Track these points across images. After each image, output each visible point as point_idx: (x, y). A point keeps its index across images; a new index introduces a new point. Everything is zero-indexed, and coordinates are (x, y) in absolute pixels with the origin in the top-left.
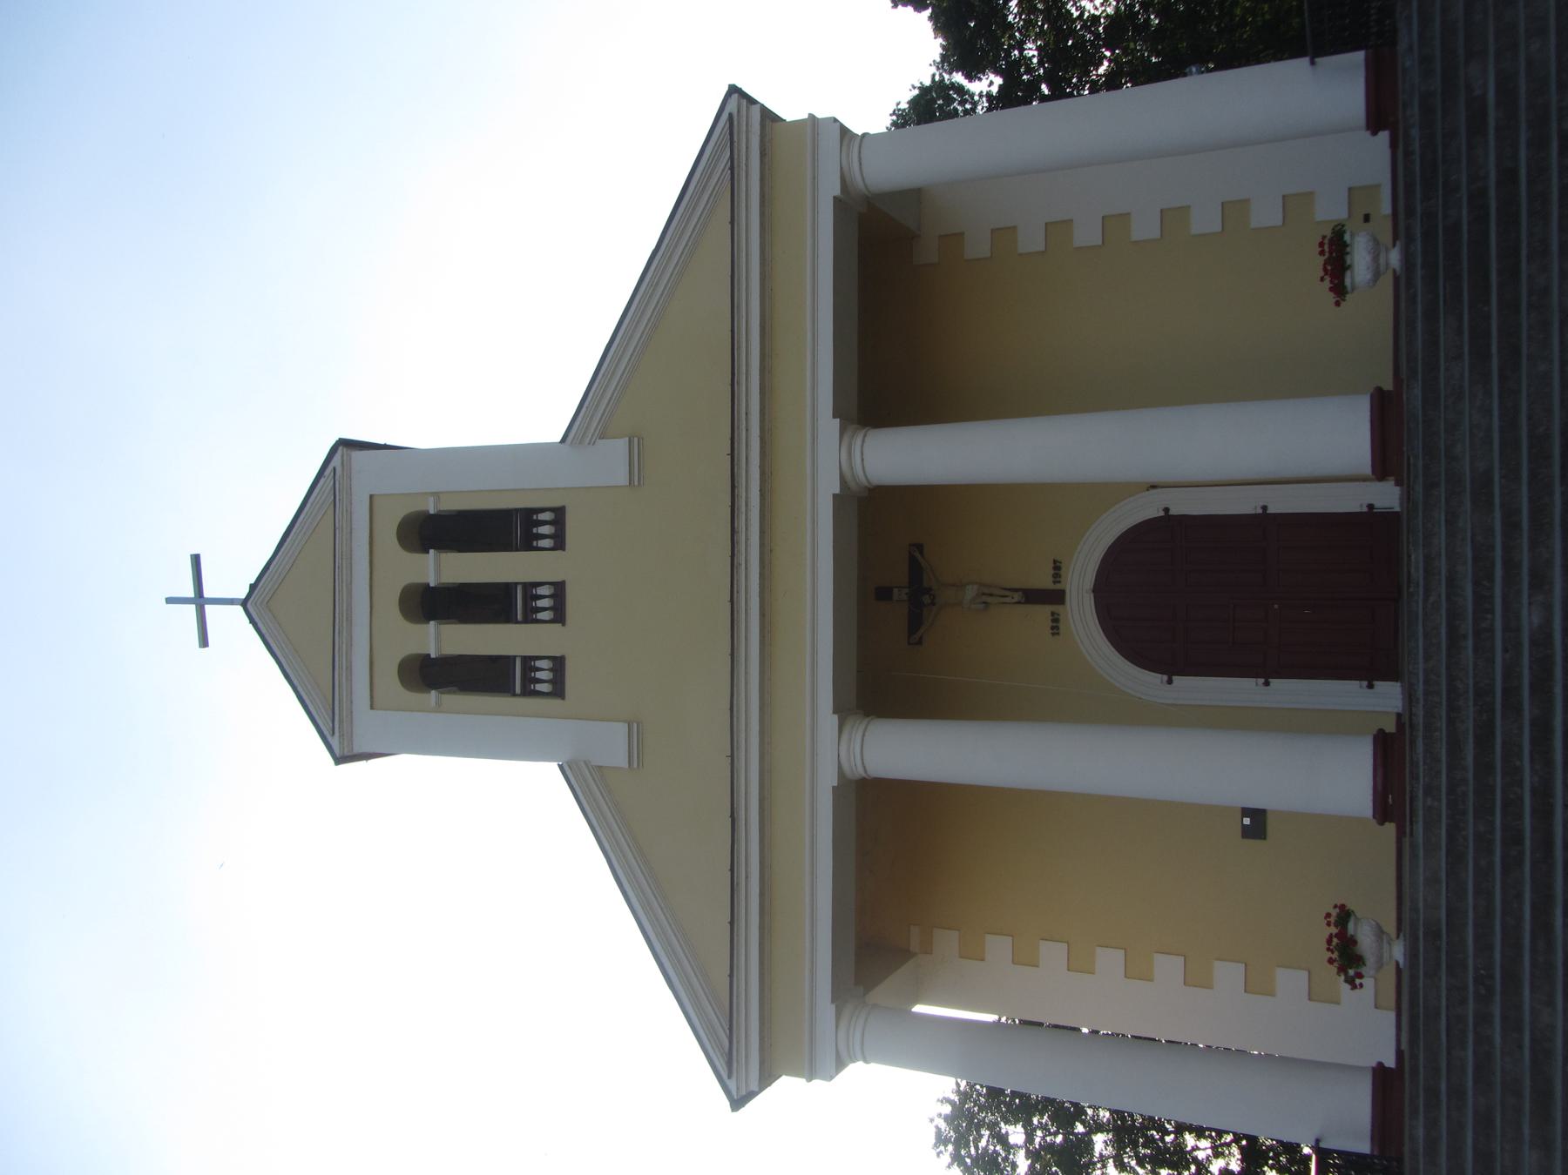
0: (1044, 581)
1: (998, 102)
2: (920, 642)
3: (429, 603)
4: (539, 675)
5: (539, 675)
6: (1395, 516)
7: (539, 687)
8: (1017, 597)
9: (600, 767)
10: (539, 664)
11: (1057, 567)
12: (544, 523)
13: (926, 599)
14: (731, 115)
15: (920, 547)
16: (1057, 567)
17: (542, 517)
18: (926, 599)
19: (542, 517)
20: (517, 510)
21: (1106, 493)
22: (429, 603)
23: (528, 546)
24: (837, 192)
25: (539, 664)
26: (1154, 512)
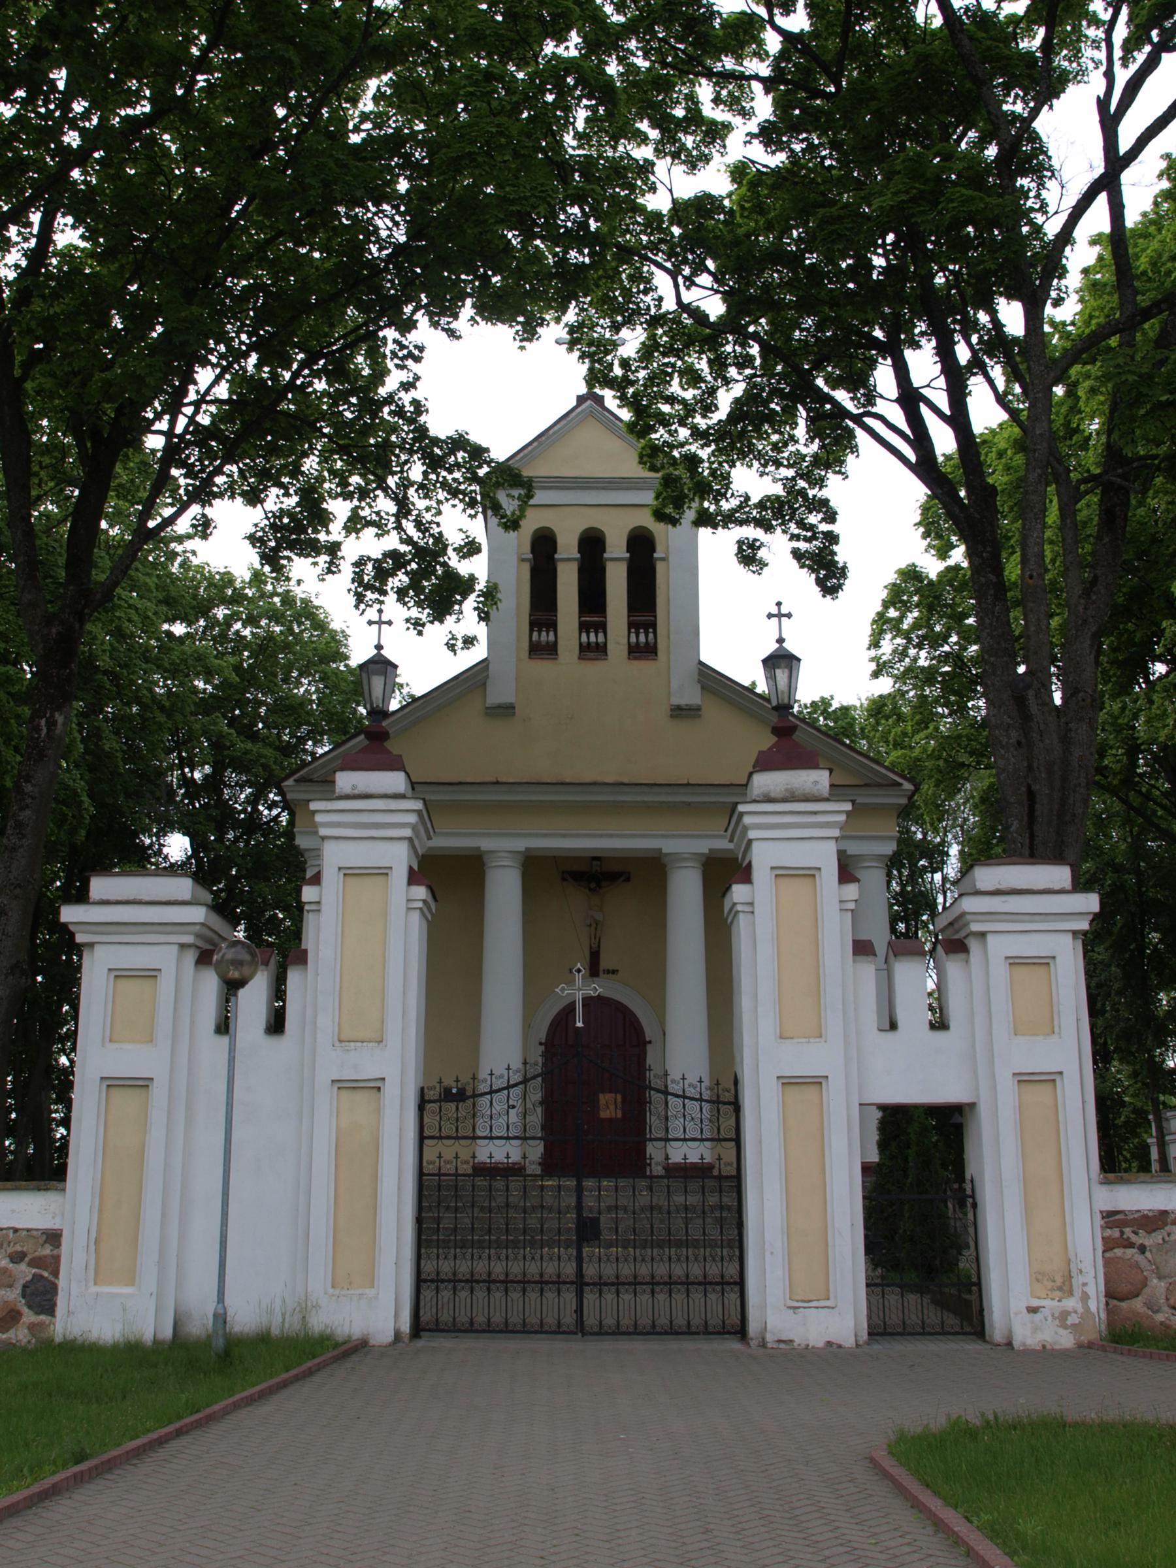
0: (605, 963)
1: (68, 1129)
2: (564, 879)
3: (592, 543)
4: (544, 634)
5: (544, 634)
6: (334, 791)
7: (535, 634)
8: (595, 946)
9: (485, 684)
10: (551, 634)
11: (614, 972)
12: (647, 637)
13: (593, 885)
14: (901, 785)
15: (628, 880)
16: (614, 972)
17: (651, 636)
18: (593, 885)
19: (651, 636)
20: (655, 617)
21: (660, 1008)
22: (592, 543)
23: (631, 625)
24: (849, 853)
25: (551, 634)
26: (649, 1035)
